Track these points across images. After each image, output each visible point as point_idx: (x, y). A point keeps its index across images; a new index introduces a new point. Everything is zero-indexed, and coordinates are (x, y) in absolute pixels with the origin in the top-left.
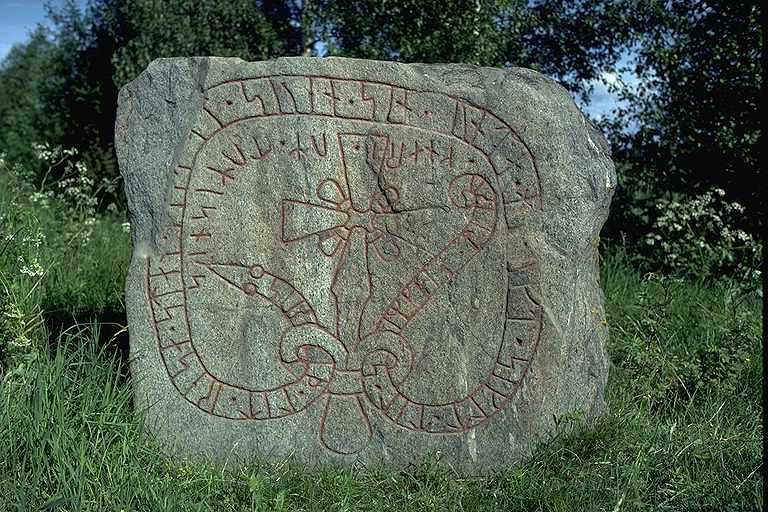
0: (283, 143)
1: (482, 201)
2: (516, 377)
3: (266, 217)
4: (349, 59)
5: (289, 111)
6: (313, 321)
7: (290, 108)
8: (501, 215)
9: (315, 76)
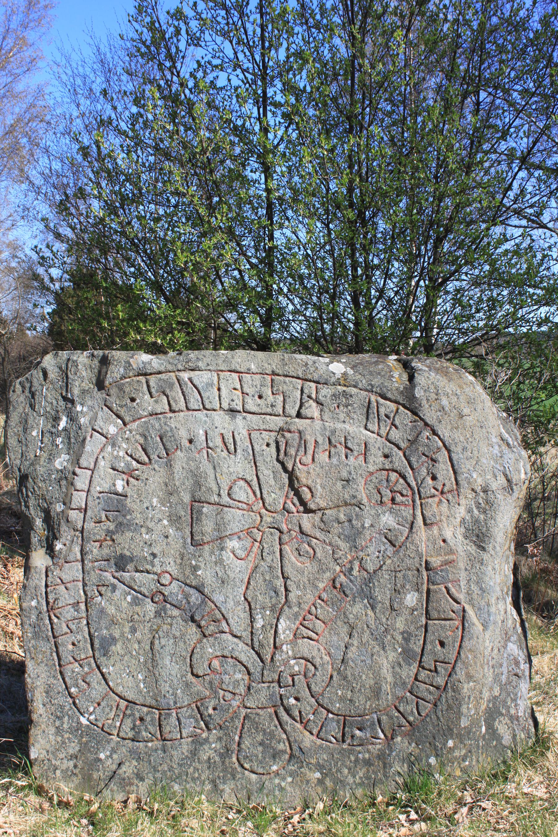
0: (191, 441)
1: (399, 498)
2: (440, 681)
3: (175, 519)
4: (203, 352)
5: (197, 408)
6: (227, 630)
7: (194, 403)
8: (418, 513)
9: (222, 371)
